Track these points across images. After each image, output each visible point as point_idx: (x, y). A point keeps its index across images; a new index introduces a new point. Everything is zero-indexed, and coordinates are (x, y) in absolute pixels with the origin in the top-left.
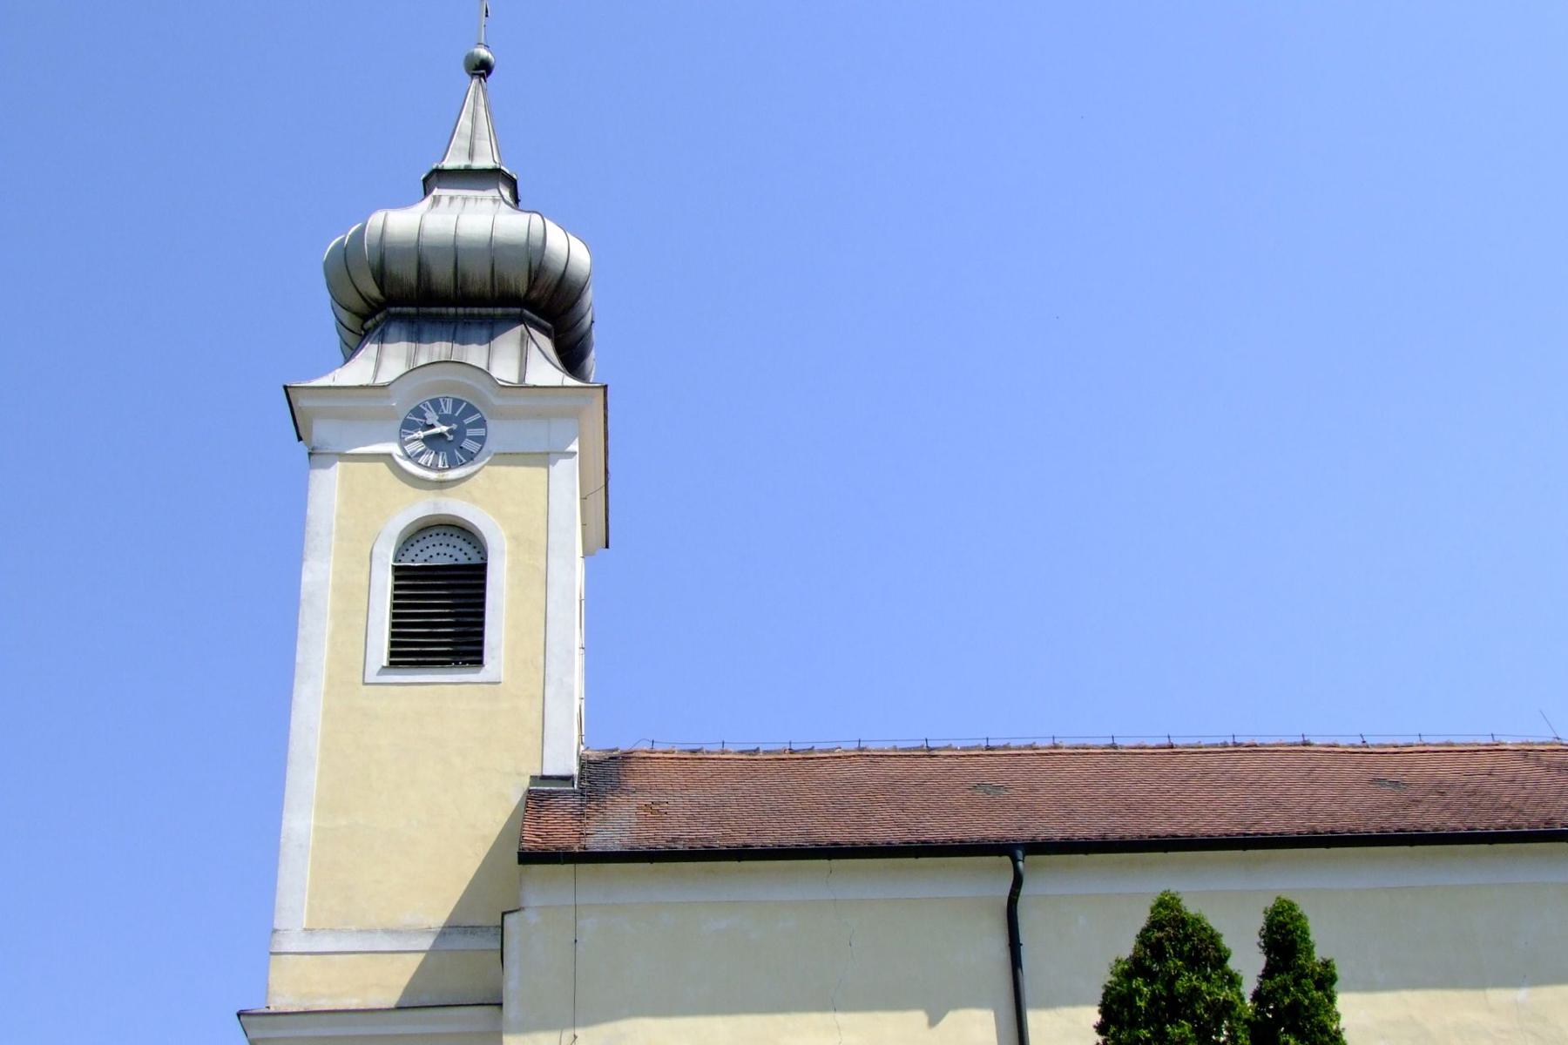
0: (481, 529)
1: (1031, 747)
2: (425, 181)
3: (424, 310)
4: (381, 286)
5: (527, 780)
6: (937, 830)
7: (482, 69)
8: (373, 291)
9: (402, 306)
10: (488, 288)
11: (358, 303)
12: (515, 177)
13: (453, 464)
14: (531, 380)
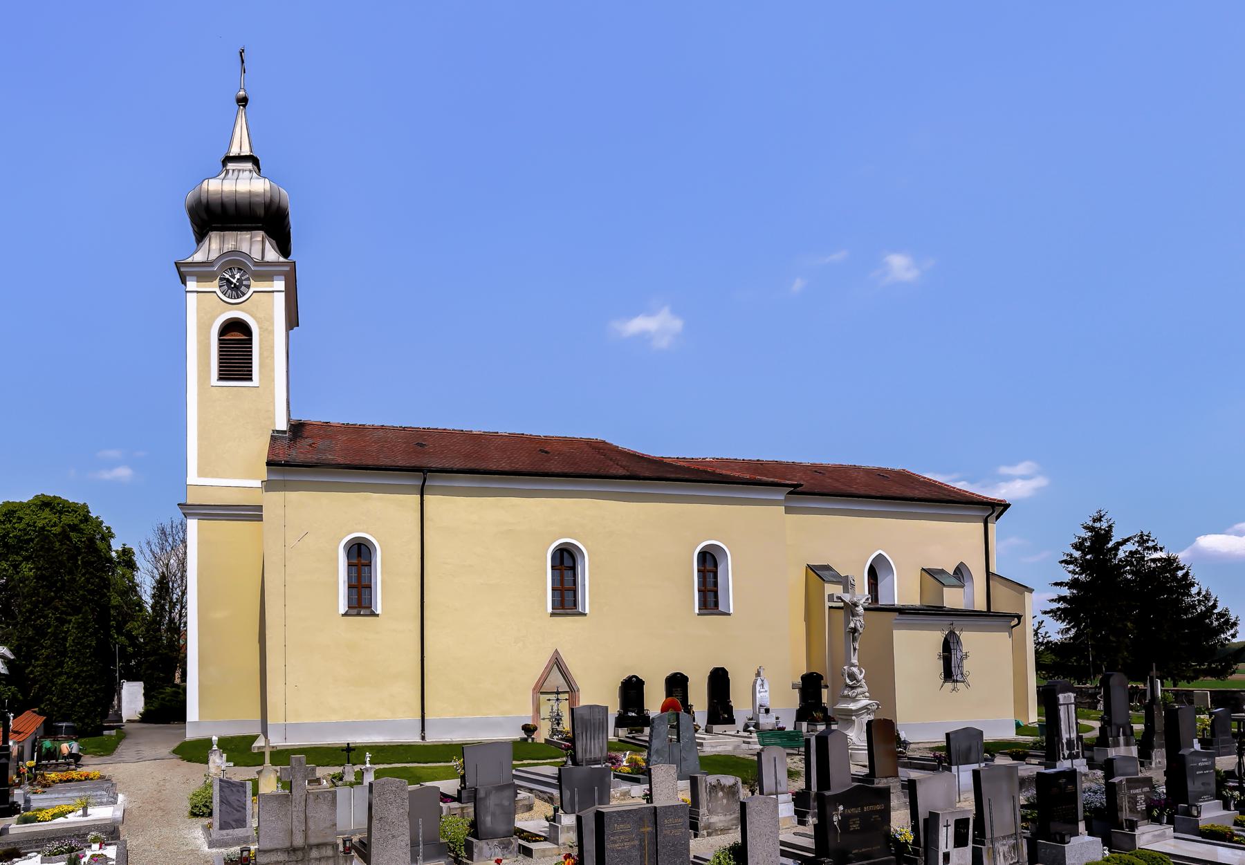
7: (243, 101)
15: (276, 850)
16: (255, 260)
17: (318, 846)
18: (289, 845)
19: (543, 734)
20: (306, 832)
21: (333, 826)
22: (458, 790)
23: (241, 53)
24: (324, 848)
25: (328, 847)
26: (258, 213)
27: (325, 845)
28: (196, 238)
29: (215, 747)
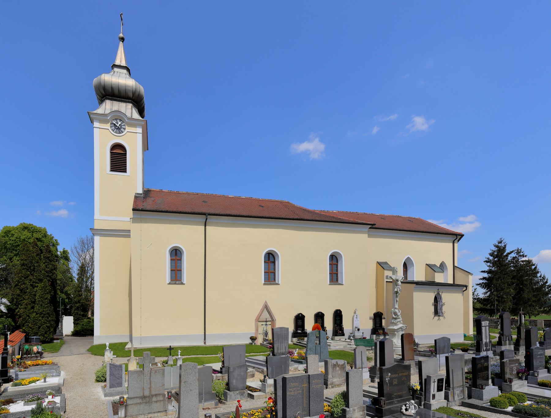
0: (123, 144)
1: (212, 194)
2: (112, 66)
3: (113, 98)
4: (104, 91)
5: (135, 194)
6: (196, 211)
7: (122, 39)
8: (104, 93)
9: (109, 96)
10: (125, 95)
11: (101, 95)
12: (129, 68)
13: (120, 133)
14: (133, 117)
15: (137, 397)
20: (150, 388)
21: (163, 385)
23: (121, 15)
26: (129, 94)
27: (159, 394)
28: (99, 102)
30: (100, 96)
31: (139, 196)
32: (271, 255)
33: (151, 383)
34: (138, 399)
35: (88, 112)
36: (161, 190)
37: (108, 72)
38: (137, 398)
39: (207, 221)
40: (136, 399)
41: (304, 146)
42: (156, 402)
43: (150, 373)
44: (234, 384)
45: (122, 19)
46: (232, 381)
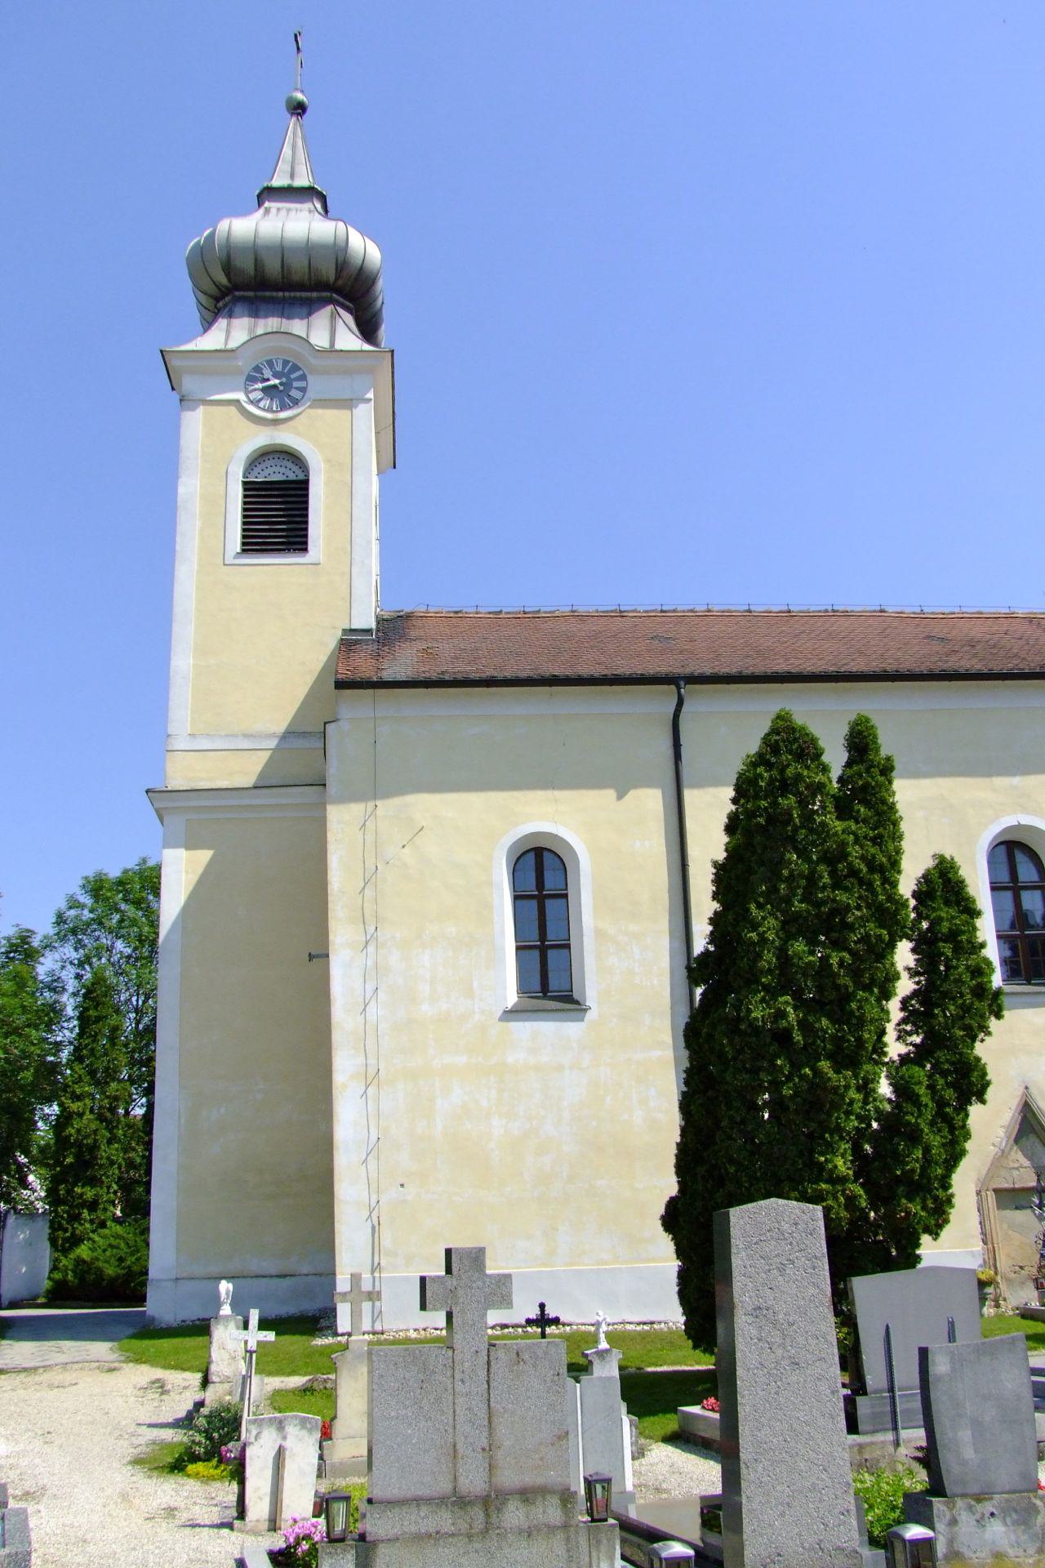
3: (260, 294)
7: (299, 109)
10: (306, 276)
15: (418, 1501)
16: (317, 348)
17: (527, 1495)
18: (450, 1487)
19: (944, 1436)
20: (490, 1450)
21: (559, 1438)
22: (999, 1016)
23: (296, 36)
24: (540, 1498)
25: (548, 1497)
26: (324, 272)
27: (542, 1491)
28: (203, 318)
29: (226, 1310)
30: (211, 296)
31: (360, 640)
32: (1020, 857)
33: (495, 1419)
34: (424, 1510)
35: (161, 351)
36: (456, 612)
37: (245, 213)
38: (418, 1505)
39: (684, 709)
40: (414, 1509)
41: (893, 1250)
42: (529, 1533)
43: (489, 1363)
44: (969, 1453)
45: (298, 48)
46: (950, 1434)
